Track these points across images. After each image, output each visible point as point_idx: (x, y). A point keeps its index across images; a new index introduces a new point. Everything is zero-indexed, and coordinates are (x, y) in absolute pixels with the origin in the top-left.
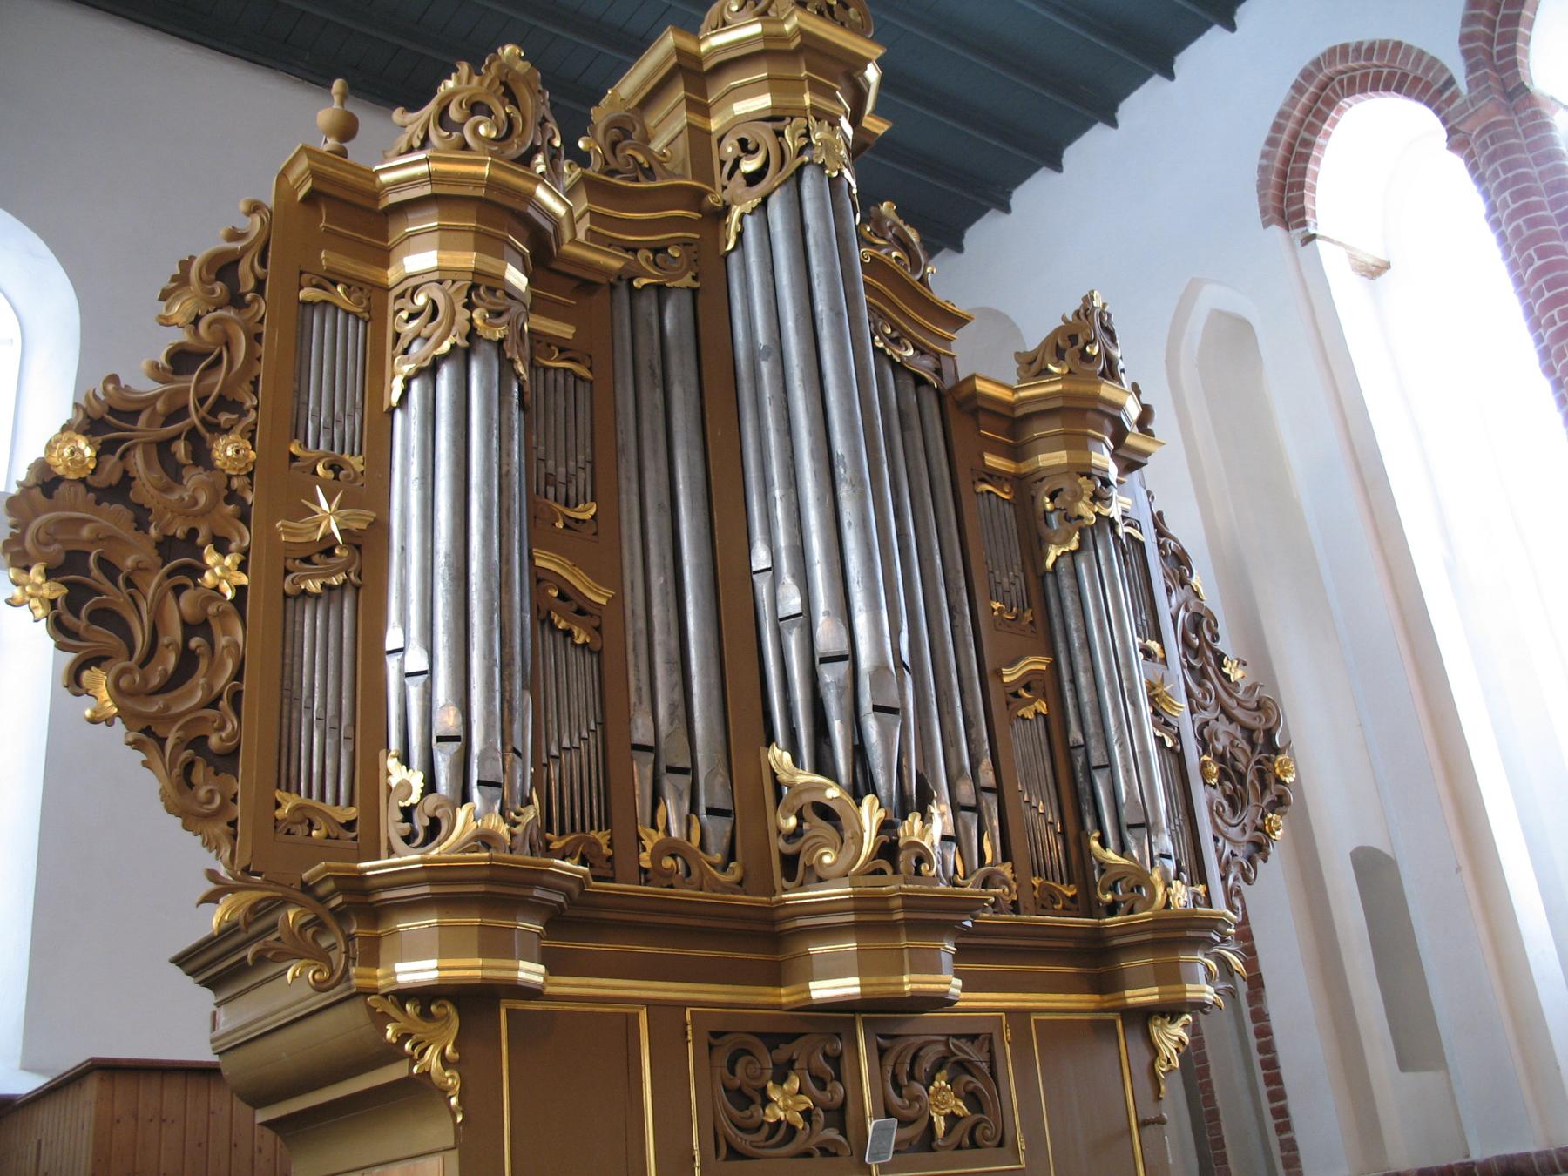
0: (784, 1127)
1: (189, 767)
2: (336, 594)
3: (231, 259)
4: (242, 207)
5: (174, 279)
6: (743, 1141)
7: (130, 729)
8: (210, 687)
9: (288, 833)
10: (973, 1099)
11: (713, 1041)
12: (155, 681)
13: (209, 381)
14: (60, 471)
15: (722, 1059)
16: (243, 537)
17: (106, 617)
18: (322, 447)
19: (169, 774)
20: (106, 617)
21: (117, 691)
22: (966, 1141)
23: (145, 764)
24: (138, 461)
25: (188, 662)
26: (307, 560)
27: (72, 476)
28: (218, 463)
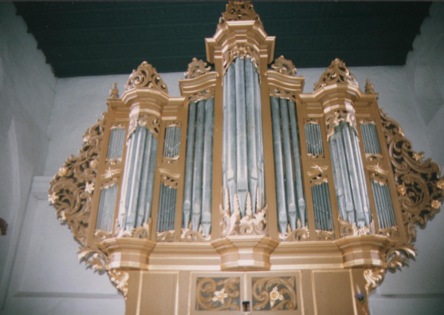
6: (203, 305)
15: (200, 284)
16: (94, 180)
17: (67, 201)
22: (282, 308)
24: (75, 171)
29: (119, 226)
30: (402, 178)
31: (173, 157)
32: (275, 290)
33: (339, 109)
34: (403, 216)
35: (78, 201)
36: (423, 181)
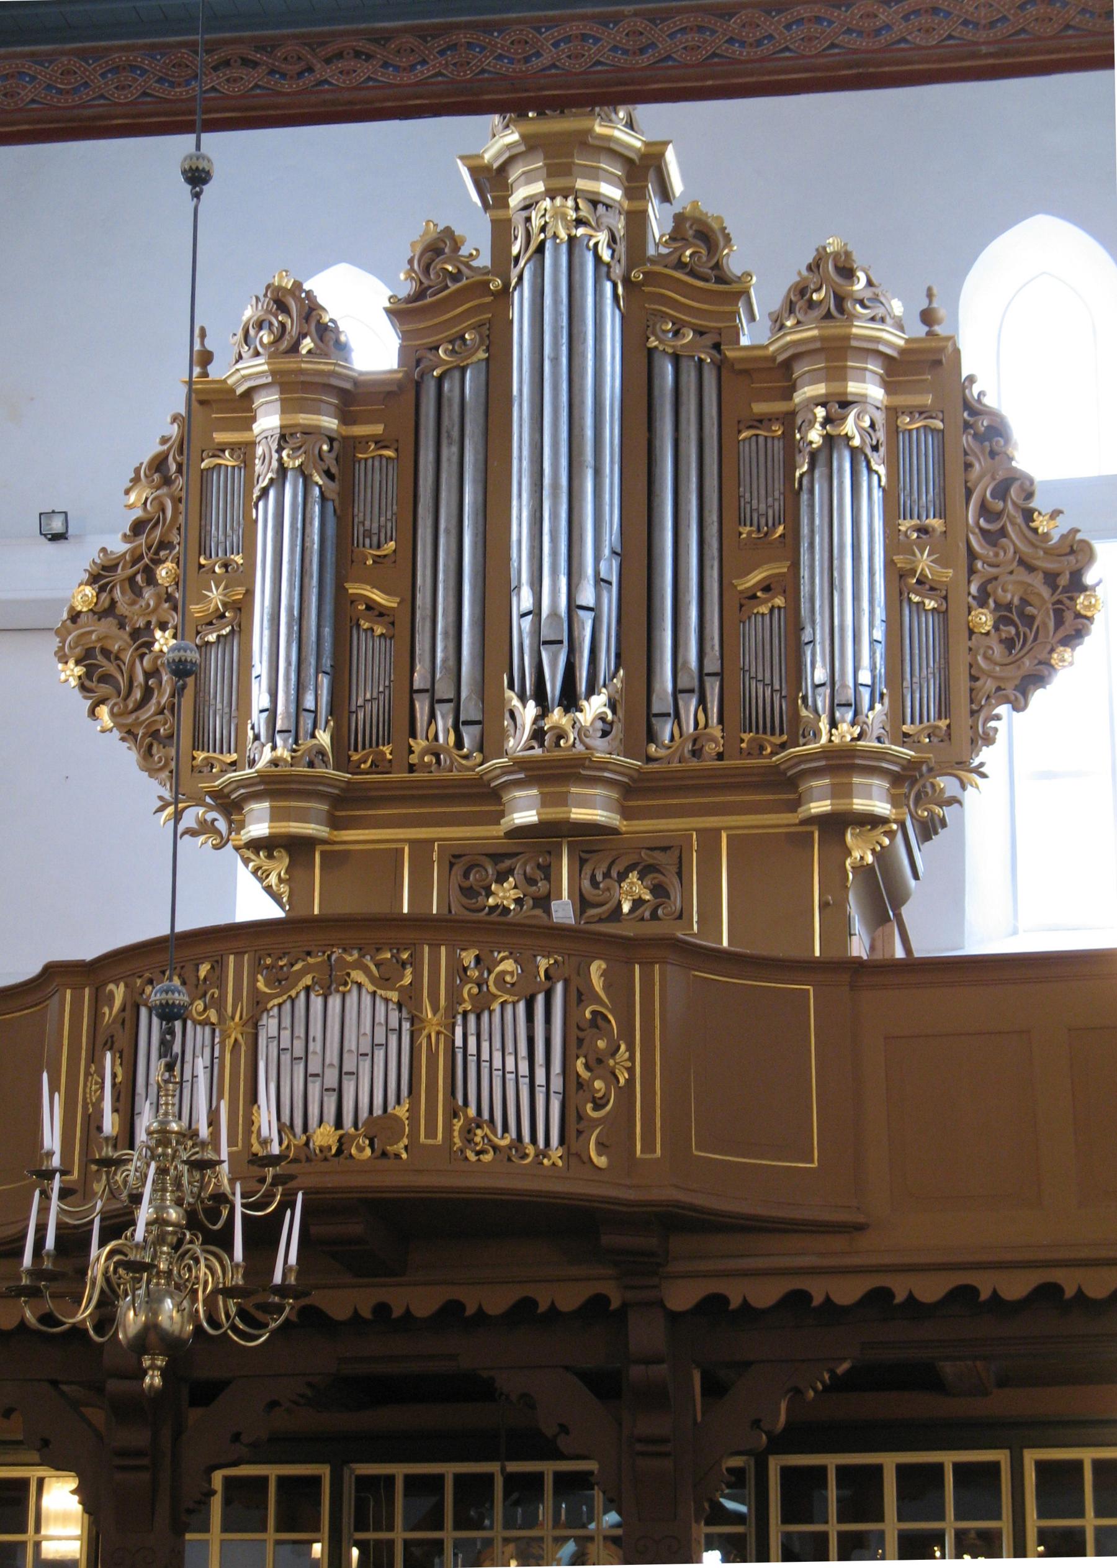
0: (501, 907)
1: (150, 746)
2: (230, 638)
3: (163, 456)
4: (169, 420)
5: (131, 481)
7: (120, 732)
8: (159, 703)
9: (200, 772)
10: (659, 890)
11: (453, 860)
12: (131, 706)
13: (153, 536)
14: (79, 608)
15: (458, 870)
17: (105, 678)
18: (220, 555)
19: (139, 752)
20: (105, 678)
21: (112, 714)
22: (647, 915)
23: (129, 748)
24: (118, 594)
25: (148, 693)
26: (211, 623)
27: (85, 609)
28: (160, 581)
29: (257, 737)
30: (989, 588)
31: (379, 547)
32: (633, 876)
33: (826, 395)
34: (972, 690)
35: (140, 677)
36: (1045, 592)
